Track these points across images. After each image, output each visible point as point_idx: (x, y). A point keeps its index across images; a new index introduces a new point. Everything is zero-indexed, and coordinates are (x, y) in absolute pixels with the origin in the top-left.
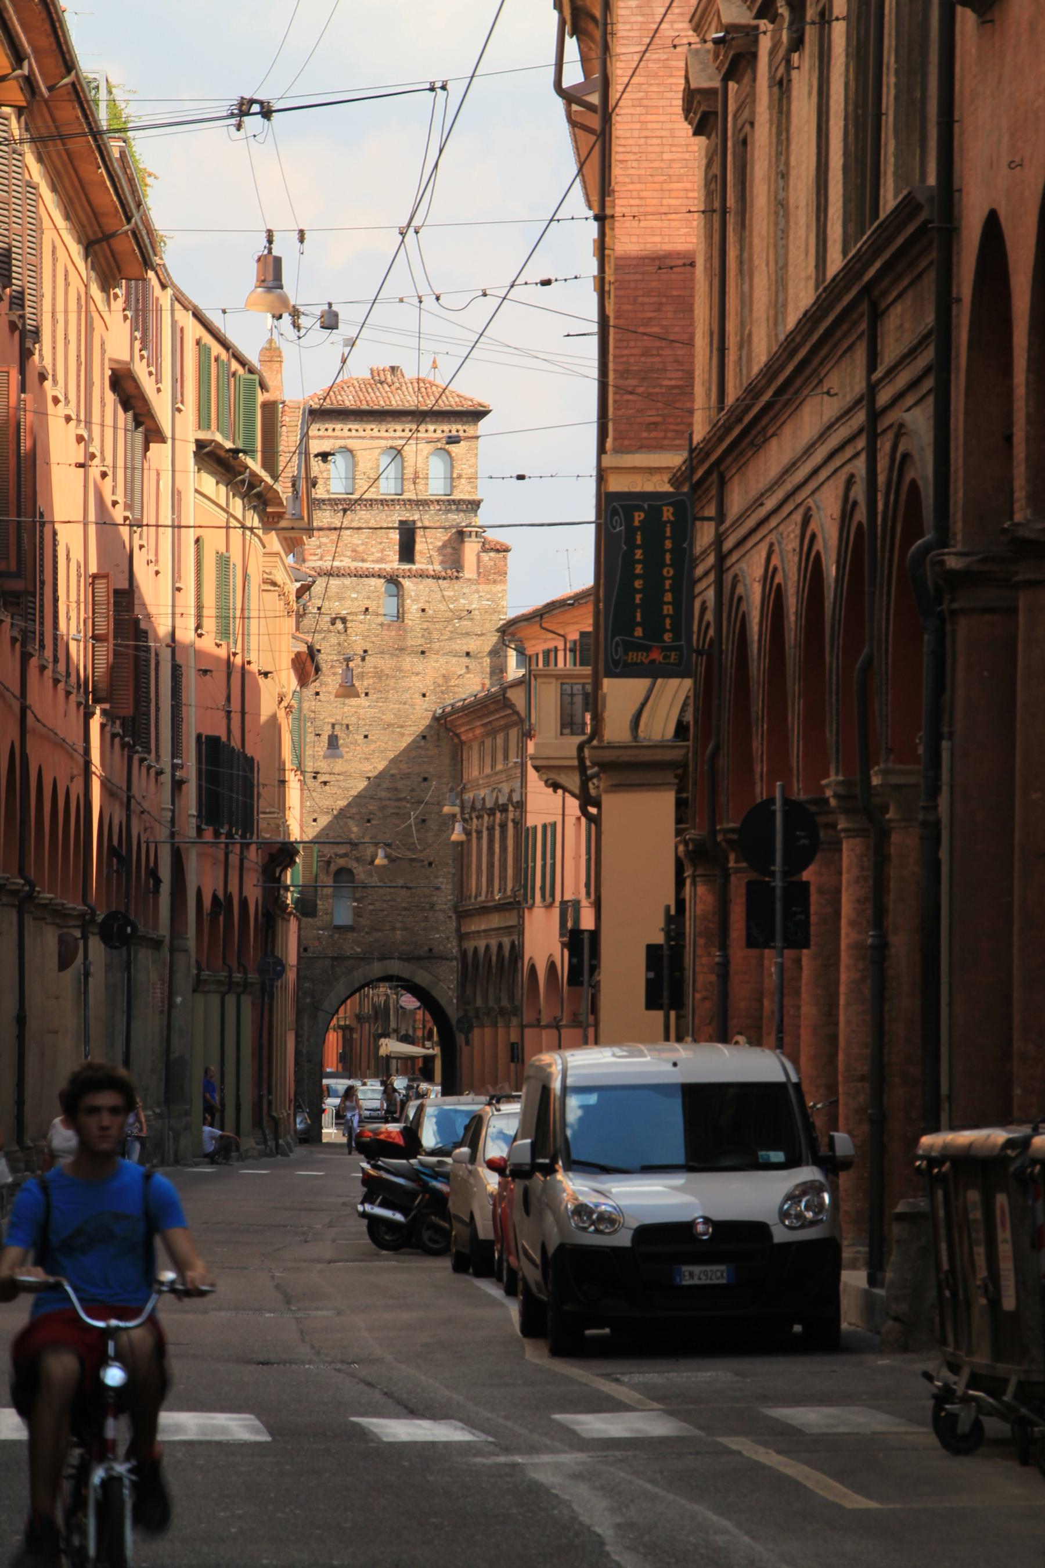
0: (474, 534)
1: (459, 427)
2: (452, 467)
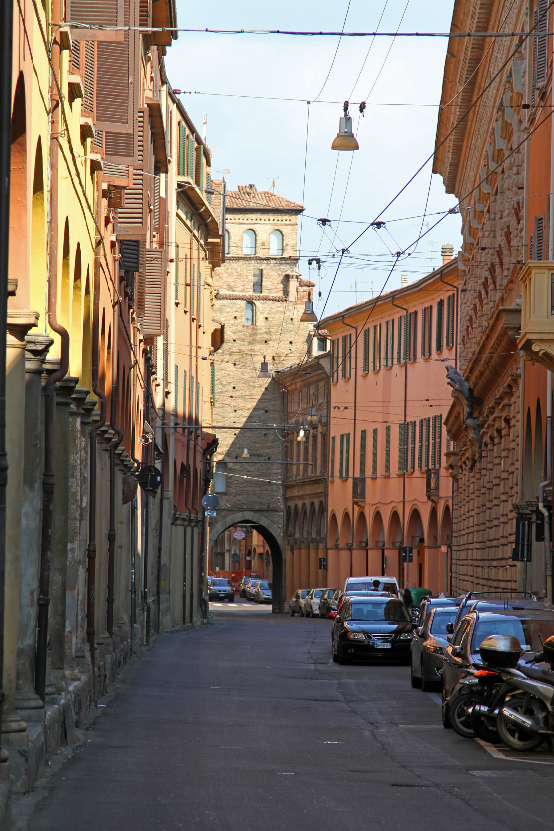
0: (295, 276)
2: (283, 240)
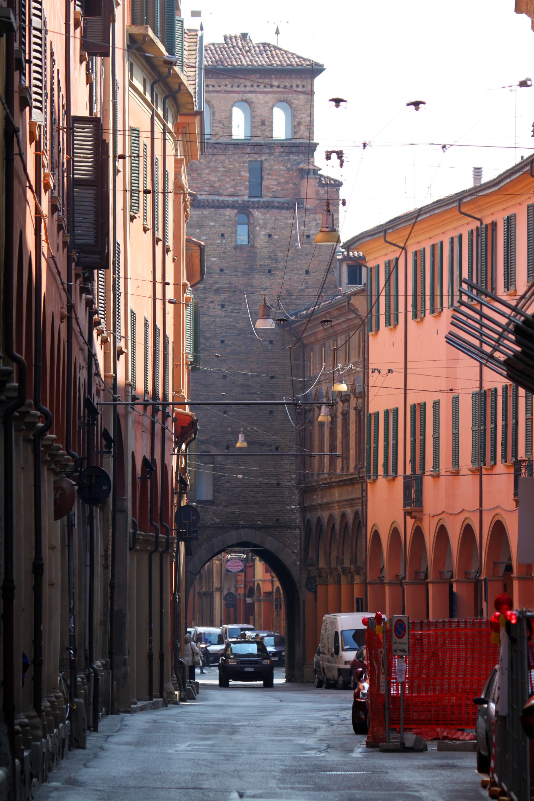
1: (299, 82)
